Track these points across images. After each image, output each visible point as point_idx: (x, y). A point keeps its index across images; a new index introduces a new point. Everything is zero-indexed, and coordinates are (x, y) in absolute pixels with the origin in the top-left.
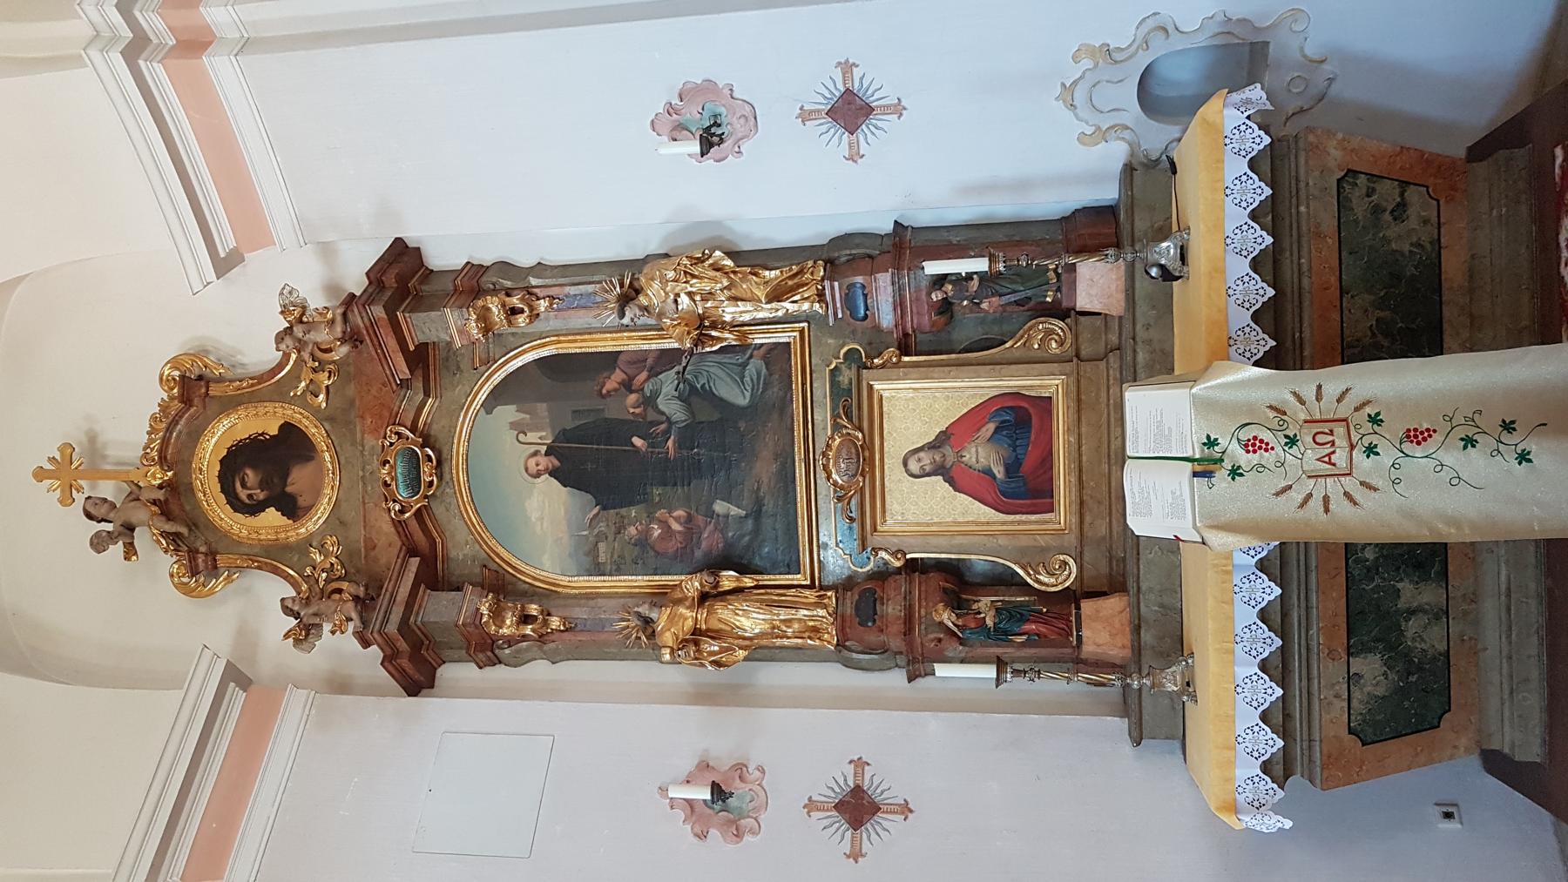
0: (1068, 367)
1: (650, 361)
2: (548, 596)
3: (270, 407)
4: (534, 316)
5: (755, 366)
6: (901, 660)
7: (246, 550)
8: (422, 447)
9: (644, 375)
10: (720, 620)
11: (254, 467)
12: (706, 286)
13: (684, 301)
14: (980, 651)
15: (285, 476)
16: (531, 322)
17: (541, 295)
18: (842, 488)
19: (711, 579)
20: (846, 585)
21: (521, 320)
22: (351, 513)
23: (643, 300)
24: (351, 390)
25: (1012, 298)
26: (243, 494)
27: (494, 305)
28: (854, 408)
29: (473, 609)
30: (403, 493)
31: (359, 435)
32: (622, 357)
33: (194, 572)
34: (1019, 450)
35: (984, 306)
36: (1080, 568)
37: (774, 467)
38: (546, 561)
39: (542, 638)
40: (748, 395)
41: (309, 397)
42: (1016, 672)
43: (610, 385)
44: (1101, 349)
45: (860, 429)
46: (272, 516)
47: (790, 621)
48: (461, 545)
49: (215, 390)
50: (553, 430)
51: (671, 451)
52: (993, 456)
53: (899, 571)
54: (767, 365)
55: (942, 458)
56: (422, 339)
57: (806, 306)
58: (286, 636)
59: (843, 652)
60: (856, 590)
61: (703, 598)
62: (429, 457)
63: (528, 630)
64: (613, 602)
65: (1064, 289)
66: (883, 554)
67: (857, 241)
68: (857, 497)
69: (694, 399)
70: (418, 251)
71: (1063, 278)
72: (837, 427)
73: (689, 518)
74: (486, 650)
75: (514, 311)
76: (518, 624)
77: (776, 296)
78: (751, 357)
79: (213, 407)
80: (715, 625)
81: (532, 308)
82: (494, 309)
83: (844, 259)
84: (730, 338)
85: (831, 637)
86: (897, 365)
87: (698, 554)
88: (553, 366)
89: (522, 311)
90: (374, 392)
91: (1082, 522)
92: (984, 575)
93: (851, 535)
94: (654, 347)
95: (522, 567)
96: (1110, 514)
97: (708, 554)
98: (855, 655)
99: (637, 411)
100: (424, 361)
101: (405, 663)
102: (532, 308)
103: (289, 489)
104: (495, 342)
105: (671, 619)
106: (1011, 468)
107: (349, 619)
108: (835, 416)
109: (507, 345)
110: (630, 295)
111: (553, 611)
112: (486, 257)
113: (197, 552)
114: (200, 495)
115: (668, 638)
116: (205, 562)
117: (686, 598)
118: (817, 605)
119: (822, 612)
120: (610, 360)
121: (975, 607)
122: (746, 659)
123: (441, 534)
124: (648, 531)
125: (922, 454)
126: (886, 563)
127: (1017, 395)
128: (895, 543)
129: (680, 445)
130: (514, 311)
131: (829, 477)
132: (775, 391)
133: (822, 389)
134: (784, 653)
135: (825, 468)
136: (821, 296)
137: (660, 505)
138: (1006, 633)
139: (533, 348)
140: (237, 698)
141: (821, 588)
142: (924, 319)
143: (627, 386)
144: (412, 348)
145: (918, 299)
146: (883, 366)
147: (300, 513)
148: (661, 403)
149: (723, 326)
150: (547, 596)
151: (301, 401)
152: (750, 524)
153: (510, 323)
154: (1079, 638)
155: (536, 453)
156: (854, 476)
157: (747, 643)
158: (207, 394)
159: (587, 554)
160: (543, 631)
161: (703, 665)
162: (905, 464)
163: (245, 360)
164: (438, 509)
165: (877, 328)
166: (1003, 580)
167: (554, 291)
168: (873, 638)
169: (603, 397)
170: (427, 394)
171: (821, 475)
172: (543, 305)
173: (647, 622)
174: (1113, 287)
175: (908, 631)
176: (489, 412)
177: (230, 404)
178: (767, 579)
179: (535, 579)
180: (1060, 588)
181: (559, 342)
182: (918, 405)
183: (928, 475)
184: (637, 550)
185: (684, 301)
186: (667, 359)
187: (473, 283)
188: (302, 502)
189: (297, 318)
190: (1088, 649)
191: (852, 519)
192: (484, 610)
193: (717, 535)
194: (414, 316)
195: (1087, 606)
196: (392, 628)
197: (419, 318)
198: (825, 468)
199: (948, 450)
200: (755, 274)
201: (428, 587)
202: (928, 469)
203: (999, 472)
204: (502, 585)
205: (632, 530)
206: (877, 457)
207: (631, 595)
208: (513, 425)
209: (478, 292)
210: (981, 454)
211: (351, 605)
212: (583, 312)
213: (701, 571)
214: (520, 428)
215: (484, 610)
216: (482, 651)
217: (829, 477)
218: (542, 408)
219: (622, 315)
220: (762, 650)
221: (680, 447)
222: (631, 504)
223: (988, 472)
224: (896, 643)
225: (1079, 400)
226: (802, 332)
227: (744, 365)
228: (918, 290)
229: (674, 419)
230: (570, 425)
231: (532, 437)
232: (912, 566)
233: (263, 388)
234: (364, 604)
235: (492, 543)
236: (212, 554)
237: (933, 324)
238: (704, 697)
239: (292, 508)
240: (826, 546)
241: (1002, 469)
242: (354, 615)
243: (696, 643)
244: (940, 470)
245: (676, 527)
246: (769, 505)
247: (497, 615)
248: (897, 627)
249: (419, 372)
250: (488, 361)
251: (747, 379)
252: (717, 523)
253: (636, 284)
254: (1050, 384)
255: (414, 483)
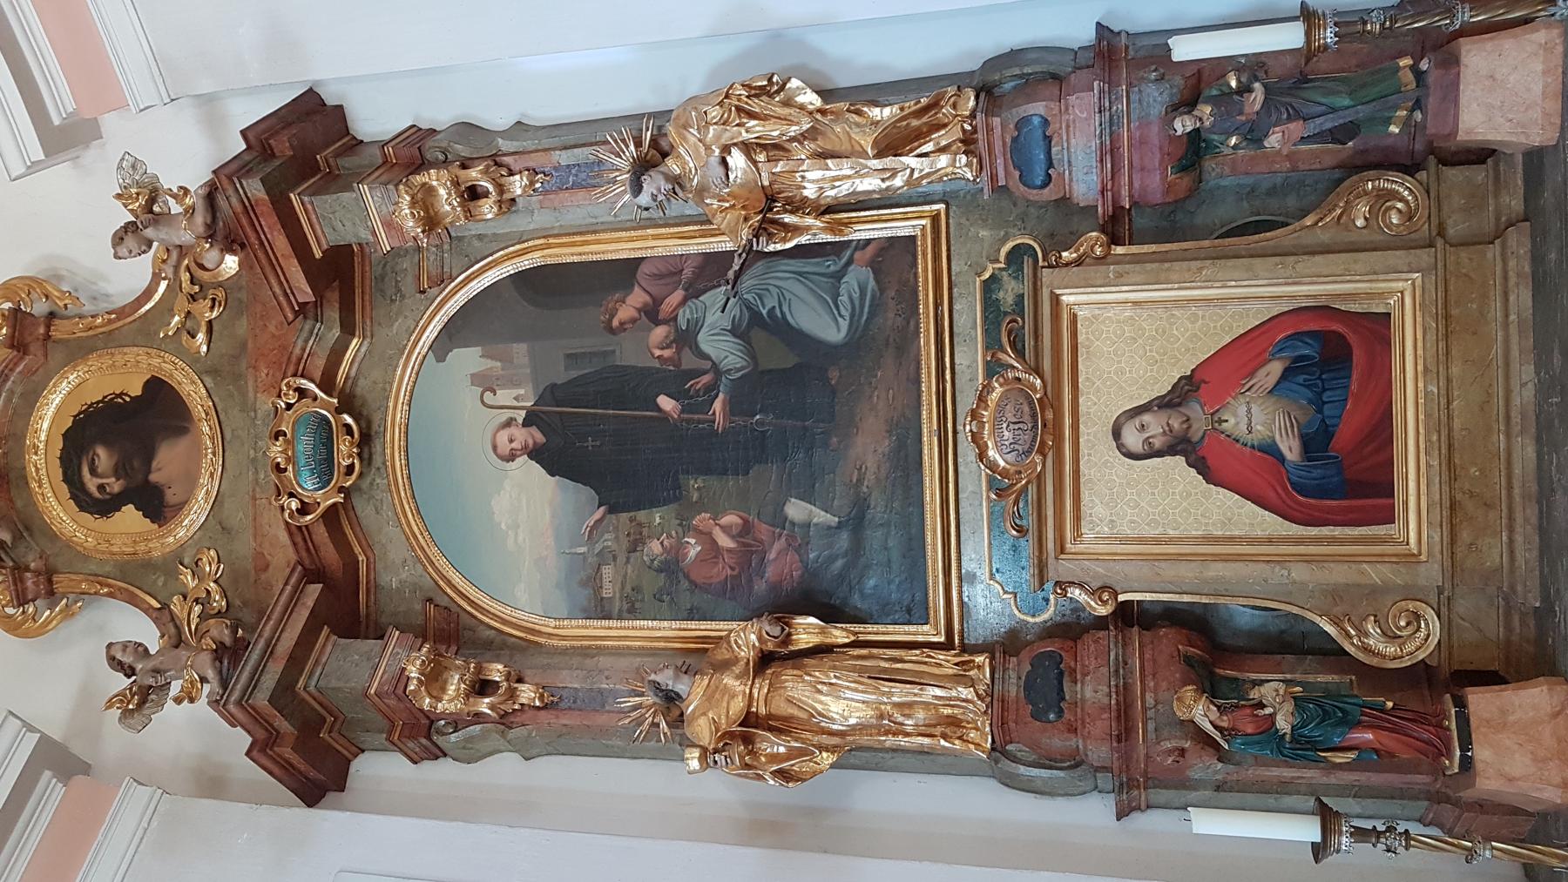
0: (1425, 256)
1: (688, 273)
2: (519, 649)
3: (132, 353)
4: (507, 204)
5: (858, 277)
6: (1104, 780)
7: (93, 568)
8: (338, 411)
9: (678, 295)
10: (789, 701)
11: (108, 444)
12: (774, 131)
13: (737, 160)
14: (1253, 773)
15: (148, 456)
16: (500, 213)
17: (516, 168)
18: (1005, 474)
19: (776, 631)
20: (1007, 645)
21: (487, 208)
22: (236, 515)
23: (672, 165)
24: (242, 327)
25: (1328, 123)
26: (92, 484)
27: (438, 182)
28: (1024, 334)
29: (395, 669)
30: (308, 485)
31: (251, 395)
32: (645, 269)
33: (21, 600)
34: (1327, 410)
35: (1273, 141)
36: (1448, 627)
37: (885, 446)
38: (522, 595)
39: (505, 720)
40: (844, 324)
41: (185, 337)
42: (1360, 834)
43: (625, 312)
44: (1489, 226)
45: (1038, 371)
46: (130, 517)
47: (910, 705)
48: (395, 560)
49: (60, 330)
50: (536, 387)
51: (719, 418)
52: (1280, 420)
53: (1101, 623)
54: (877, 273)
55: (1181, 422)
56: (334, 239)
57: (943, 160)
58: (110, 704)
59: (1002, 759)
60: (1026, 656)
61: (765, 661)
62: (348, 426)
63: (484, 705)
64: (624, 663)
65: (1432, 102)
66: (1075, 593)
67: (1033, 56)
68: (1032, 490)
69: (758, 335)
70: (340, 108)
71: (1431, 79)
72: (993, 369)
73: (746, 528)
74: (421, 736)
75: (474, 194)
76: (467, 696)
77: (893, 143)
78: (850, 262)
79: (57, 355)
80: (781, 707)
81: (501, 189)
82: (442, 192)
83: (1008, 86)
84: (815, 231)
85: (981, 736)
86: (1101, 260)
87: (760, 587)
88: (542, 286)
89: (486, 194)
90: (272, 328)
91: (1453, 542)
92: (1251, 633)
93: (1017, 560)
94: (693, 250)
95: (484, 601)
96: (1511, 530)
97: (774, 587)
98: (1022, 769)
99: (667, 353)
100: (341, 277)
101: (287, 752)
102: (501, 189)
103: (153, 477)
104: (450, 248)
105: (709, 697)
106: (1314, 442)
107: (203, 680)
108: (992, 344)
109: (468, 254)
110: (653, 156)
111: (528, 674)
112: (439, 114)
113: (27, 569)
114: (34, 485)
115: (702, 730)
116: (36, 584)
117: (736, 660)
118: (959, 679)
119: (966, 693)
120: (624, 272)
121: (1254, 694)
122: (832, 766)
123: (368, 547)
124: (680, 547)
125: (1146, 418)
126: (1078, 608)
127: (1324, 311)
128: (1099, 572)
129: (733, 408)
130: (474, 194)
131: (982, 456)
132: (890, 318)
133: (969, 314)
134: (899, 759)
135: (976, 438)
136: (968, 143)
137: (700, 507)
138: (1314, 746)
139: (509, 257)
140: (51, 793)
141: (964, 649)
142: (1152, 179)
143: (651, 313)
144: (318, 254)
145: (1143, 142)
146: (1078, 262)
147: (168, 512)
148: (705, 342)
149: (798, 205)
150: (522, 650)
151: (174, 345)
152: (844, 540)
153: (469, 215)
154: (1467, 764)
155: (509, 423)
156: (1028, 452)
157: (835, 740)
158: (47, 337)
159: (584, 584)
160: (508, 707)
161: (760, 777)
162: (1117, 434)
163: (110, 289)
164: (364, 509)
165: (1064, 202)
166: (1289, 643)
167: (534, 161)
168: (1058, 742)
169: (612, 331)
170: (348, 329)
171: (968, 452)
172: (517, 185)
173: (671, 699)
174: (1537, 89)
175: (1124, 730)
176: (441, 358)
177: (79, 350)
178: (873, 632)
179: (504, 622)
180: (1406, 663)
181: (549, 246)
182: (1134, 330)
183: (1159, 454)
184: (661, 579)
185: (737, 160)
186: (713, 268)
187: (413, 153)
188: (171, 497)
189: (147, 208)
190: (1488, 783)
191: (1021, 530)
192: (413, 672)
193: (791, 557)
194: (317, 200)
195: (1480, 701)
196: (261, 699)
197: (325, 202)
198: (976, 438)
199: (1195, 410)
200: (859, 113)
201: (333, 631)
202: (1158, 443)
203: (1290, 449)
204: (450, 631)
205: (655, 547)
206: (1067, 421)
207: (653, 652)
208: (477, 379)
209: (420, 164)
210: (1258, 417)
211: (206, 658)
212: (581, 194)
213: (759, 616)
214: (486, 383)
215: (413, 672)
216: (412, 737)
217: (982, 456)
218: (520, 350)
219: (637, 188)
220: (860, 752)
221: (732, 413)
222: (653, 504)
223: (1270, 450)
224: (1099, 752)
225: (1447, 317)
226: (935, 219)
227: (839, 276)
228: (1144, 123)
229: (724, 366)
230: (561, 375)
231: (505, 396)
232: (1127, 615)
233: (129, 326)
234: (228, 655)
235: (441, 563)
236: (48, 574)
237: (1169, 188)
238: (765, 830)
239: (157, 506)
240: (972, 578)
241: (1296, 444)
242: (210, 674)
243: (747, 740)
244: (1179, 445)
245: (725, 541)
246: (878, 509)
247: (434, 678)
248: (1102, 725)
249: (333, 296)
250: (441, 280)
251: (844, 298)
252: (791, 537)
253: (664, 144)
254: (1400, 292)
255: (325, 467)
